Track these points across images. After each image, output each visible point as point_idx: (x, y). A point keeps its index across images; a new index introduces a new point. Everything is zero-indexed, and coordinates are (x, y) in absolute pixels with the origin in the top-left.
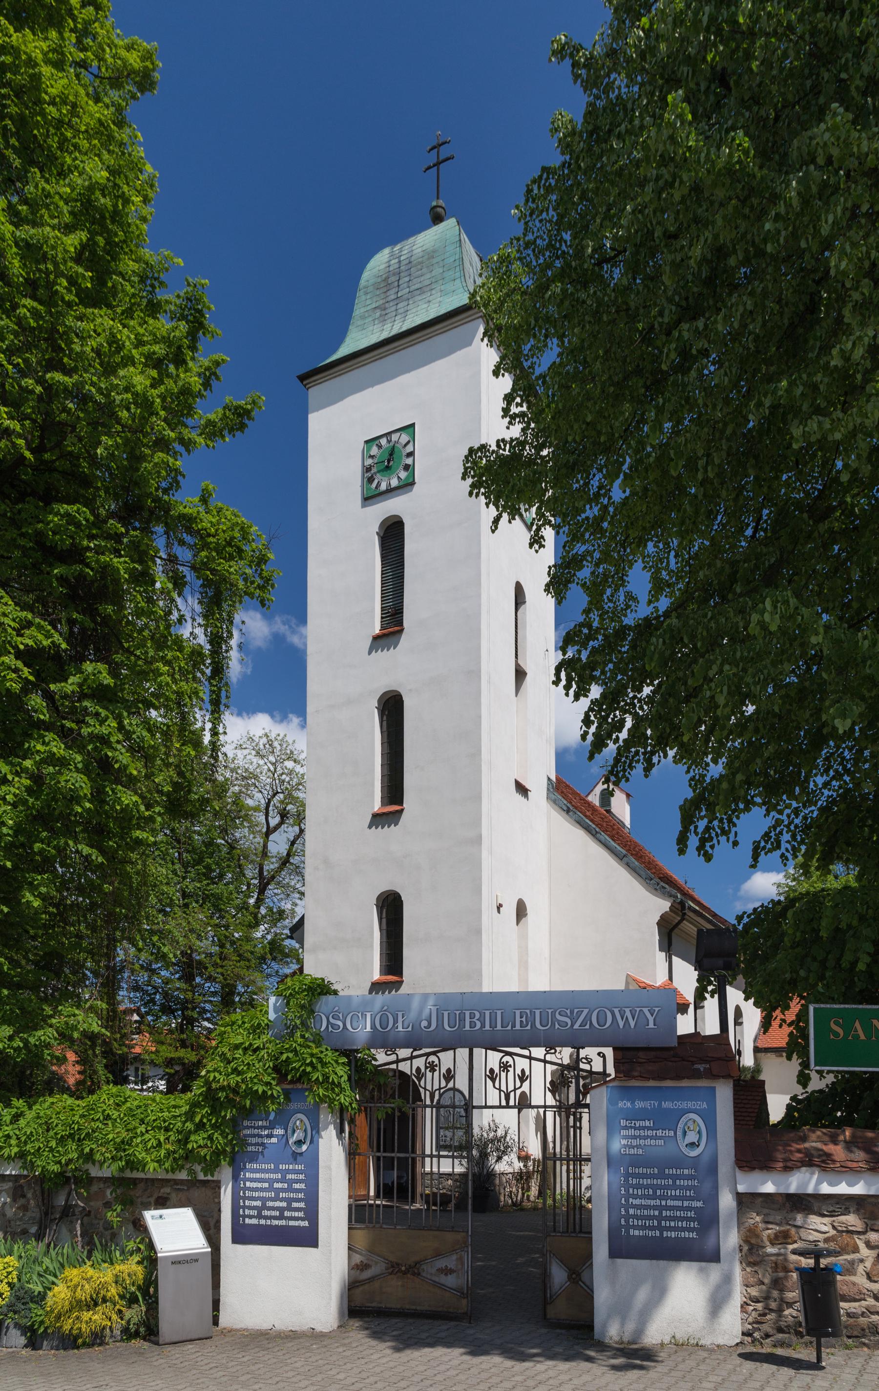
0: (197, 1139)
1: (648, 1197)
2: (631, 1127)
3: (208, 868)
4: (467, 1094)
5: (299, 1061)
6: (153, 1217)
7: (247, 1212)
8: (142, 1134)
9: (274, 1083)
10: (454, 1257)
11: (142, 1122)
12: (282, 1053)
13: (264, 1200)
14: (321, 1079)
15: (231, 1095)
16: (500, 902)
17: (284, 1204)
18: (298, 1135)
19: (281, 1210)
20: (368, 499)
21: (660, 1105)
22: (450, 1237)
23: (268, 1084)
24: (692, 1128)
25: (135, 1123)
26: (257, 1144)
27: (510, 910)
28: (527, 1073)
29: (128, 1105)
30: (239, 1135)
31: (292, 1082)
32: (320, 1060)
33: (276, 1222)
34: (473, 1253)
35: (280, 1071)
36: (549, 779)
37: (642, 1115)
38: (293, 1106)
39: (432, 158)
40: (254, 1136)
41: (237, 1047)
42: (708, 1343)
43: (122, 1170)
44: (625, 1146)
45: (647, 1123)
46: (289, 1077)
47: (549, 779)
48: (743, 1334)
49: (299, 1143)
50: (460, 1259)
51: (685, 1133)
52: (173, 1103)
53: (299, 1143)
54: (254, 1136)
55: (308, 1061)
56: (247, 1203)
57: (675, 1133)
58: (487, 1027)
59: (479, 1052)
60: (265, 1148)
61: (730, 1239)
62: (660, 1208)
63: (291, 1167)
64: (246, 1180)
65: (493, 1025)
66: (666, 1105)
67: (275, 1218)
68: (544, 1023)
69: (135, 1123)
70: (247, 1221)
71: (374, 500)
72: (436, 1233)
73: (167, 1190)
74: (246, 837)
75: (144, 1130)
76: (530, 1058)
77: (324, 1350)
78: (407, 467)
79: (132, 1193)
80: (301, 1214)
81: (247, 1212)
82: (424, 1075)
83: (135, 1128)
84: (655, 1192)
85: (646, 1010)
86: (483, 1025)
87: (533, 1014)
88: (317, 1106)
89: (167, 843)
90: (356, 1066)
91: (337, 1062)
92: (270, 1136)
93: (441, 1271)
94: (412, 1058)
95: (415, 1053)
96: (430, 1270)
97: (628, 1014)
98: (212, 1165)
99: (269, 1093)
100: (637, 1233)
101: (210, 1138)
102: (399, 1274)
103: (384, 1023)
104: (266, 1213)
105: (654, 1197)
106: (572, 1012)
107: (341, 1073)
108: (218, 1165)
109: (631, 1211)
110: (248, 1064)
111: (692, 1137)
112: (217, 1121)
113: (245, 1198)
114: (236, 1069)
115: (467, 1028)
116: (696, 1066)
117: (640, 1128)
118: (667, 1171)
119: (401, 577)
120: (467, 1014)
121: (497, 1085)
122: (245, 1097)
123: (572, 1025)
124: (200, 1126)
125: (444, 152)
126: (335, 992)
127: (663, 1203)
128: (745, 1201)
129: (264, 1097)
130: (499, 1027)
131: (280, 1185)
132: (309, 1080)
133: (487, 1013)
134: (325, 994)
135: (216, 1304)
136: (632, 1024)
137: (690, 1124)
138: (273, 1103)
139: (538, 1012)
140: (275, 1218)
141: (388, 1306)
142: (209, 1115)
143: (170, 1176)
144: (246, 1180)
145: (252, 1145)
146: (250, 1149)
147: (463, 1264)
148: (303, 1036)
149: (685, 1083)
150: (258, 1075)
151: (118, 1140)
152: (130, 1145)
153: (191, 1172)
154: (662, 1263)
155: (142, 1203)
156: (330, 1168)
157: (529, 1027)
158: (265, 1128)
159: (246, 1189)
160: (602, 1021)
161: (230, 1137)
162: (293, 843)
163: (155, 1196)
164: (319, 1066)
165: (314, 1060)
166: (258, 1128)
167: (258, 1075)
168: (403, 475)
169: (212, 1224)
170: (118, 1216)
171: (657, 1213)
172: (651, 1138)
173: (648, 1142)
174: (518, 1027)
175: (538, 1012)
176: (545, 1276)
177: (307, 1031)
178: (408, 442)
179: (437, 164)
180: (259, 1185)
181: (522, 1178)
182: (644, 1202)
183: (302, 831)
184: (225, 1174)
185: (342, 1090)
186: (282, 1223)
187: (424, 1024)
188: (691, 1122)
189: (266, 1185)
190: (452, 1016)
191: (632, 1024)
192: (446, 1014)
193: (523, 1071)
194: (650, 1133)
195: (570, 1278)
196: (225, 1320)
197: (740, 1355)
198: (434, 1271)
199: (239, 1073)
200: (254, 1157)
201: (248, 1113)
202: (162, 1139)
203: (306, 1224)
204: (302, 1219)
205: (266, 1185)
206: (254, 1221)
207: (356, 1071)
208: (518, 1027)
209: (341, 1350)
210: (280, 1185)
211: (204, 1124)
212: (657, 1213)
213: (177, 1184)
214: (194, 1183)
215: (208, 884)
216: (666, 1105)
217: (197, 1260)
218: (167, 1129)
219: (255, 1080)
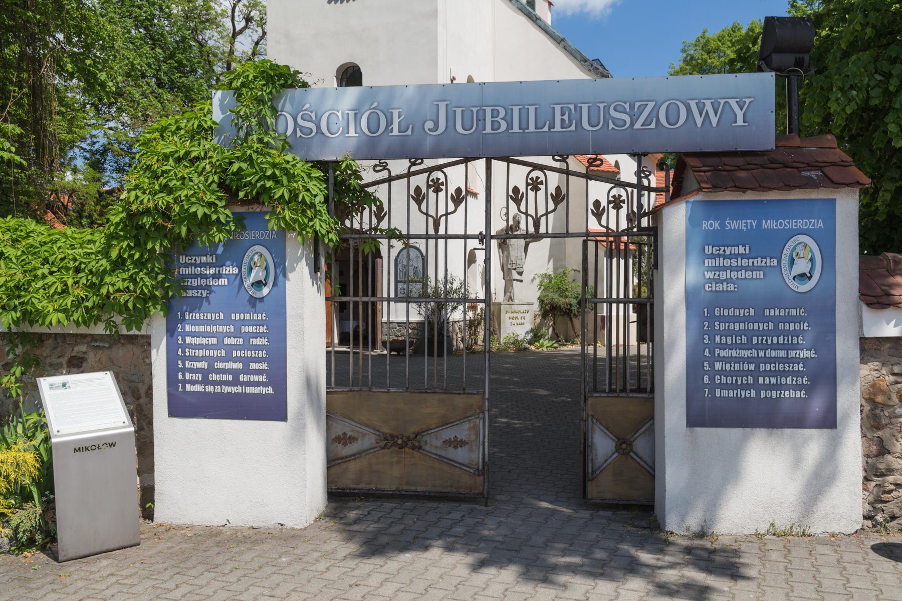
0: (116, 281)
1: (742, 347)
2: (719, 256)
3: (179, 62)
4: (424, 254)
5: (256, 173)
6: (51, 386)
7: (188, 376)
8: (44, 277)
9: (221, 204)
10: (466, 426)
11: (46, 261)
12: (231, 163)
13: (211, 360)
14: (287, 196)
15: (160, 221)
16: (453, 75)
17: (239, 366)
18: (257, 274)
19: (235, 373)
21: (759, 225)
22: (460, 401)
23: (211, 204)
24: (803, 252)
25: (36, 263)
26: (198, 288)
28: (564, 191)
29: (31, 240)
30: (173, 275)
31: (244, 202)
32: (286, 172)
33: (228, 389)
34: (509, 430)
35: (229, 188)
37: (738, 238)
38: (248, 235)
40: (195, 276)
41: (166, 157)
42: (819, 531)
43: (17, 322)
44: (710, 281)
45: (741, 250)
46: (241, 194)
48: (865, 518)
49: (259, 284)
50: (475, 428)
51: (792, 262)
52: (89, 237)
53: (259, 284)
54: (195, 276)
55: (269, 173)
56: (188, 364)
57: (779, 262)
58: (516, 129)
59: (498, 167)
60: (211, 292)
61: (850, 400)
62: (757, 361)
63: (247, 316)
64: (185, 334)
65: (524, 126)
66: (767, 224)
67: (227, 383)
68: (594, 122)
69: (36, 263)
70: (189, 387)
72: (443, 396)
73: (83, 348)
74: (213, 38)
75: (46, 271)
76: (567, 172)
77: (298, 567)
79: (38, 352)
80: (263, 378)
81: (188, 376)
82: (426, 196)
83: (35, 269)
84: (750, 340)
85: (733, 102)
86: (510, 126)
87: (579, 110)
88: (282, 233)
89: (141, 39)
90: (335, 185)
91: (309, 175)
92: (218, 276)
93: (448, 442)
94: (409, 175)
95: (413, 169)
96: (433, 442)
97: (709, 107)
98: (138, 316)
99: (214, 217)
100: (725, 393)
101: (132, 279)
102: (395, 448)
103: (373, 126)
104: (214, 377)
105: (749, 346)
106: (632, 107)
107: (315, 191)
108: (147, 315)
109: (718, 366)
110: (183, 178)
111: (802, 266)
112: (142, 256)
113: (184, 358)
114: (166, 185)
115: (488, 129)
116: (804, 174)
117: (731, 257)
118: (767, 312)
120: (488, 111)
121: (523, 208)
122: (180, 222)
123: (632, 124)
124: (119, 264)
126: (305, 85)
127: (761, 354)
128: (870, 348)
129: (206, 223)
130: (532, 128)
131: (232, 341)
132: (271, 198)
133: (516, 110)
134: (292, 86)
135: (148, 494)
136: (714, 120)
137: (800, 249)
138: (220, 231)
139: (585, 108)
140: (227, 383)
141: (380, 487)
142: (131, 248)
143: (83, 330)
144: (185, 334)
145: (193, 288)
146: (190, 293)
147: (477, 435)
148: (260, 141)
149: (796, 195)
150: (197, 192)
151: (11, 284)
152: (26, 290)
153: (110, 324)
154: (735, 433)
155: (51, 365)
156: (301, 317)
157: (573, 128)
158: (211, 265)
159: (185, 346)
160: (672, 119)
161: (160, 277)
162: (257, 43)
163: (67, 356)
164: (285, 180)
165: (277, 172)
166: (201, 265)
167: (197, 192)
169: (142, 391)
170: (17, 381)
171: (752, 367)
172: (747, 269)
173: (742, 274)
174: (558, 127)
175: (585, 108)
176: (585, 446)
177: (267, 134)
180: (204, 341)
181: (472, 325)
182: (734, 353)
183: (264, 33)
184: (156, 325)
185: (317, 213)
186: (238, 389)
187: (429, 125)
188: (801, 247)
189: (214, 341)
190: (467, 114)
191: (714, 120)
192: (459, 112)
193: (558, 189)
194: (745, 262)
195: (618, 449)
196: (165, 510)
197: (877, 549)
198: (439, 443)
199: (171, 191)
200: (196, 305)
201: (187, 245)
202: (70, 282)
203: (270, 390)
204: (264, 385)
205: (214, 341)
206: (198, 388)
207: (335, 191)
208: (558, 127)
209: (322, 566)
210: (232, 341)
211: (124, 260)
212: (752, 367)
213: (96, 341)
214: (116, 339)
215: (180, 77)
216: (767, 224)
217: (112, 445)
218: (78, 270)
219: (193, 200)
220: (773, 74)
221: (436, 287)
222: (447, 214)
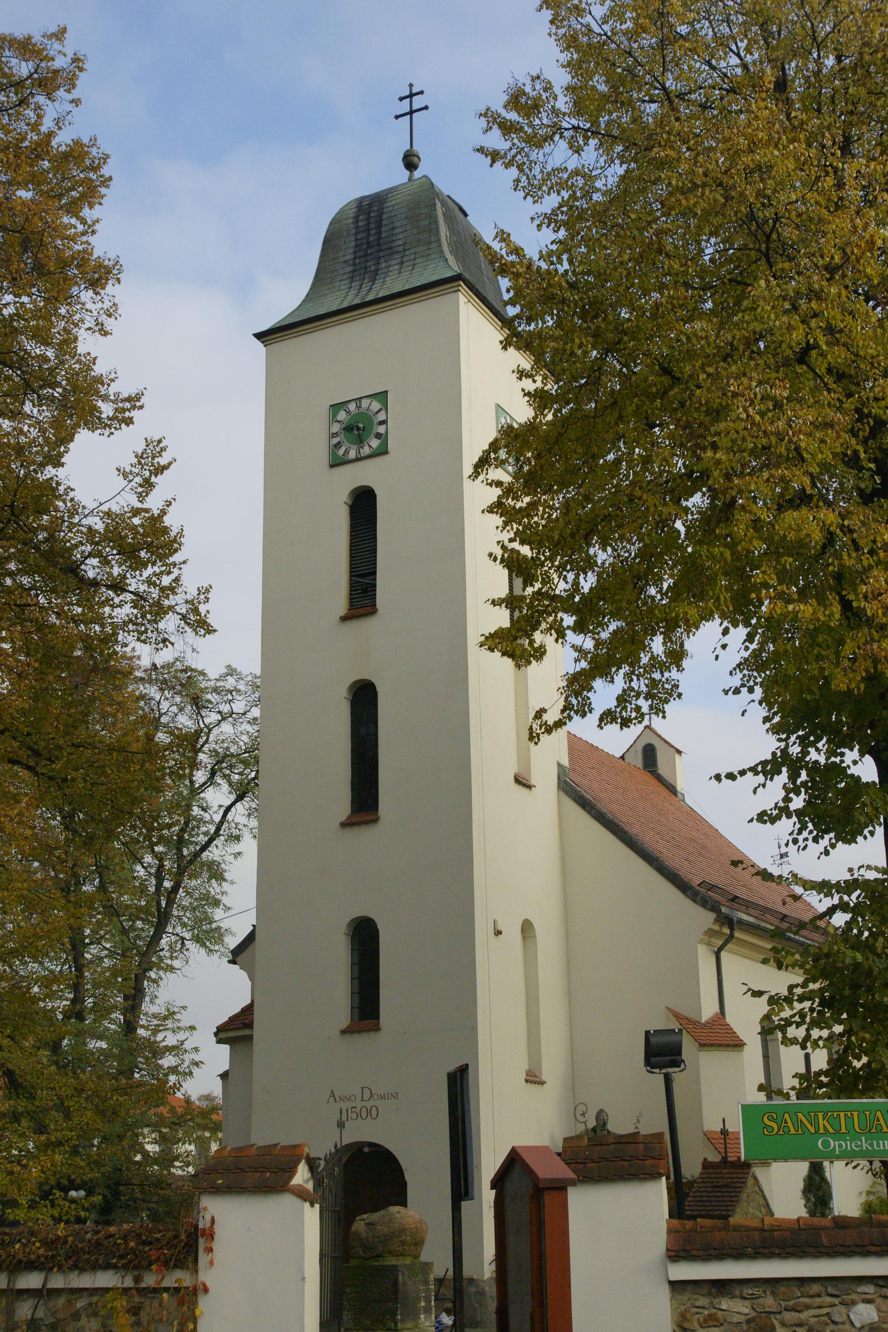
20: (336, 463)
27: (512, 932)
39: (405, 106)
71: (468, 1141)
78: (378, 436)
125: (418, 102)
168: (375, 443)
178: (380, 410)
179: (411, 112)
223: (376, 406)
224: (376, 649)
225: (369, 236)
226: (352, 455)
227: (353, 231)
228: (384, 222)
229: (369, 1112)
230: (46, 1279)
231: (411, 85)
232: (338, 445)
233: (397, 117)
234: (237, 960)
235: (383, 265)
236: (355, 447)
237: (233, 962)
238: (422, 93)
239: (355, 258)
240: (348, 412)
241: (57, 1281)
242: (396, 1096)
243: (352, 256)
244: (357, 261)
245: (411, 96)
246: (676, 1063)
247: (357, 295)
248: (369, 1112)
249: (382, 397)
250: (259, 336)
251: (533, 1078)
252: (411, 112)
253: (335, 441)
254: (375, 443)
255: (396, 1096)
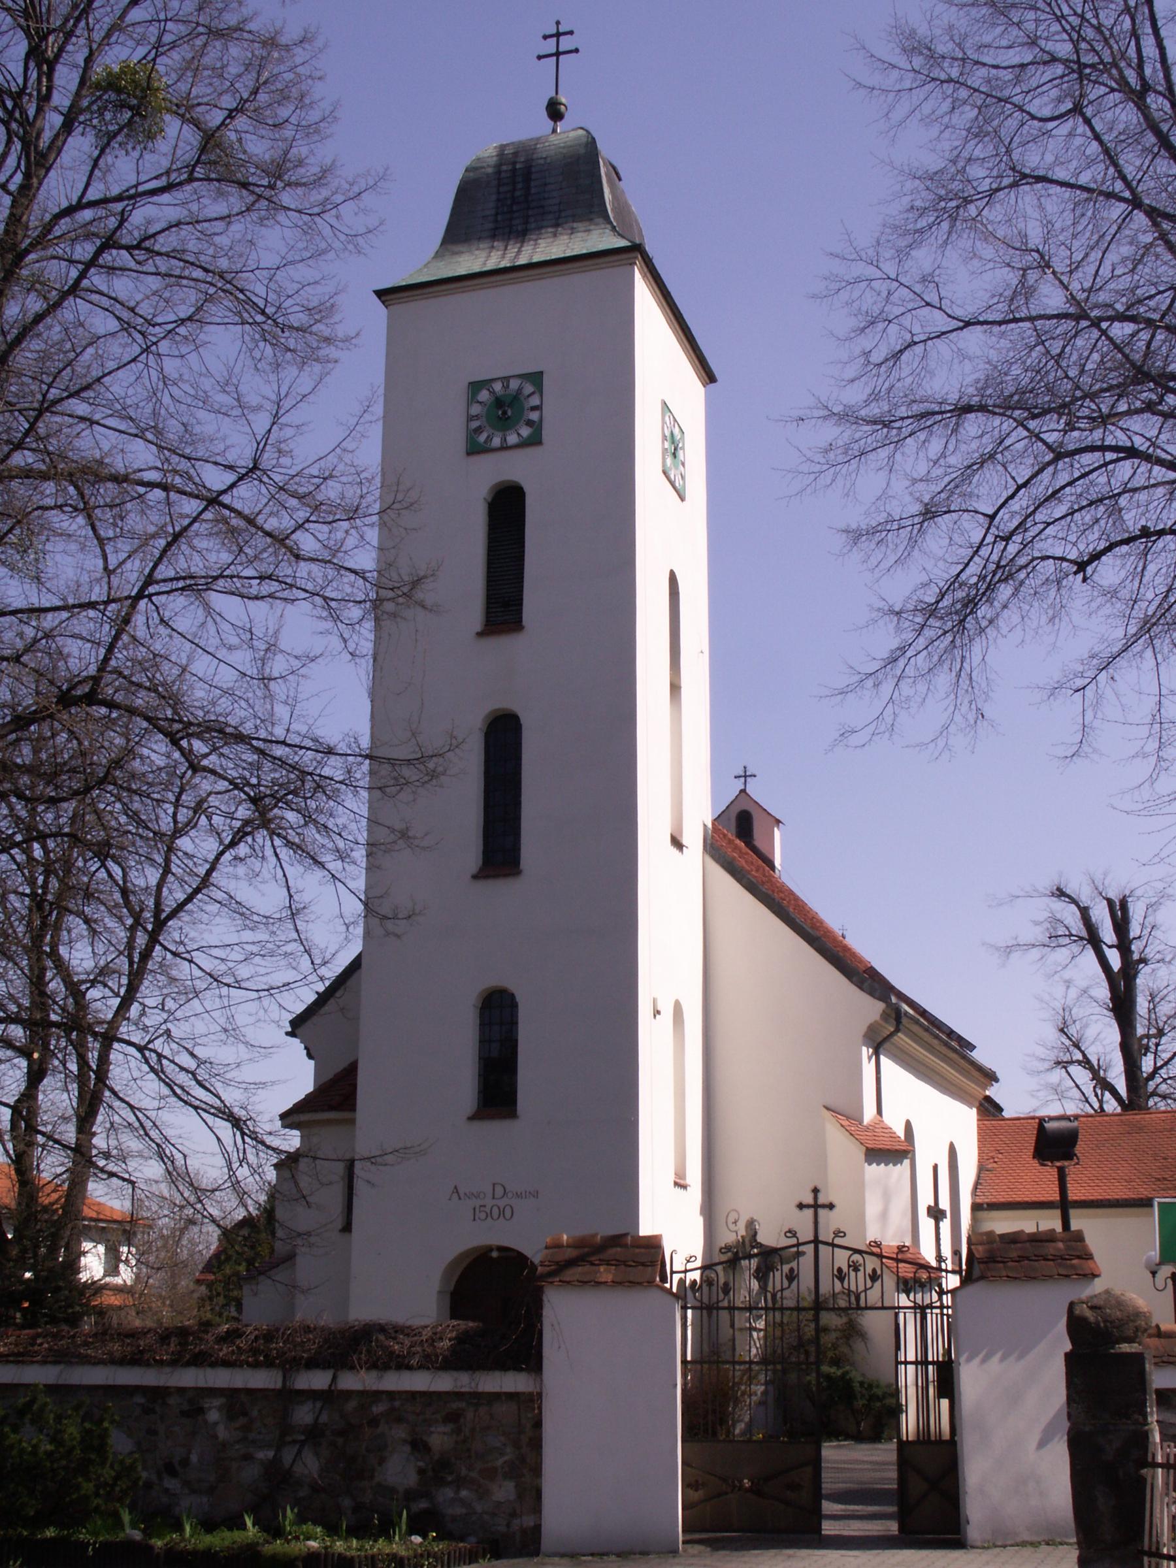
20: (474, 449)
28: (879, 1272)
36: (705, 825)
39: (550, 46)
47: (705, 825)
78: (530, 423)
119: (739, 880)
125: (566, 43)
168: (525, 432)
178: (533, 393)
179: (558, 54)
193: (874, 1270)
220: (641, 1234)
221: (783, 1353)
222: (866, 1290)
223: (529, 389)
224: (518, 674)
225: (514, 190)
226: (496, 442)
227: (495, 183)
228: (534, 176)
229: (502, 1213)
230: (334, 1378)
231: (558, 23)
232: (478, 430)
233: (539, 58)
234: (297, 1032)
235: (533, 226)
236: (500, 434)
237: (291, 1034)
238: (571, 33)
239: (497, 214)
240: (492, 392)
241: (350, 1381)
242: (536, 1195)
243: (493, 212)
244: (500, 218)
245: (558, 35)
246: (1069, 1155)
247: (503, 256)
248: (502, 1213)
249: (536, 378)
250: (381, 294)
251: (680, 1185)
252: (558, 54)
253: (475, 424)
254: (525, 432)
255: (536, 1195)
